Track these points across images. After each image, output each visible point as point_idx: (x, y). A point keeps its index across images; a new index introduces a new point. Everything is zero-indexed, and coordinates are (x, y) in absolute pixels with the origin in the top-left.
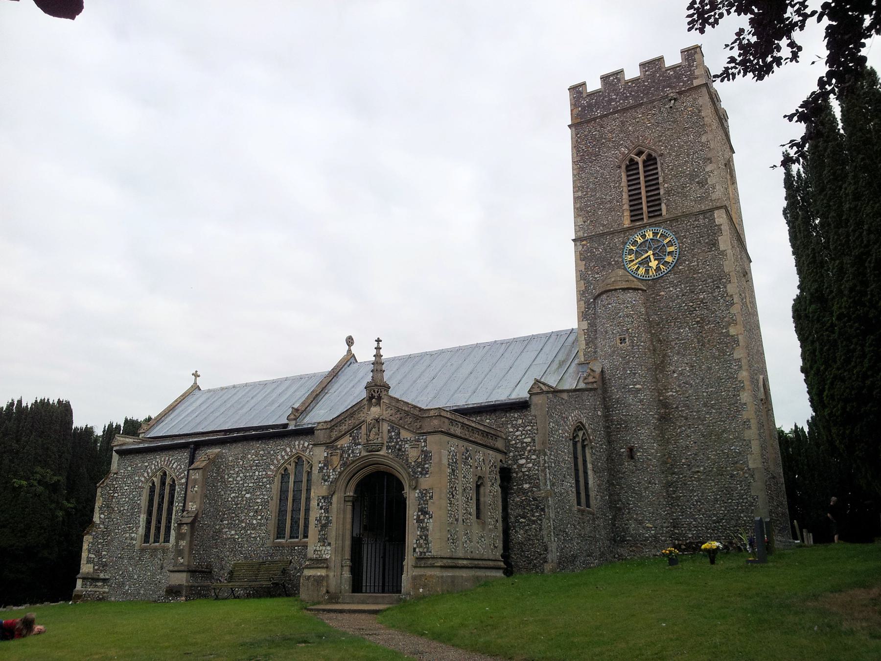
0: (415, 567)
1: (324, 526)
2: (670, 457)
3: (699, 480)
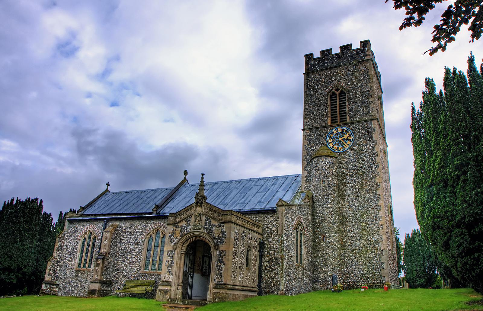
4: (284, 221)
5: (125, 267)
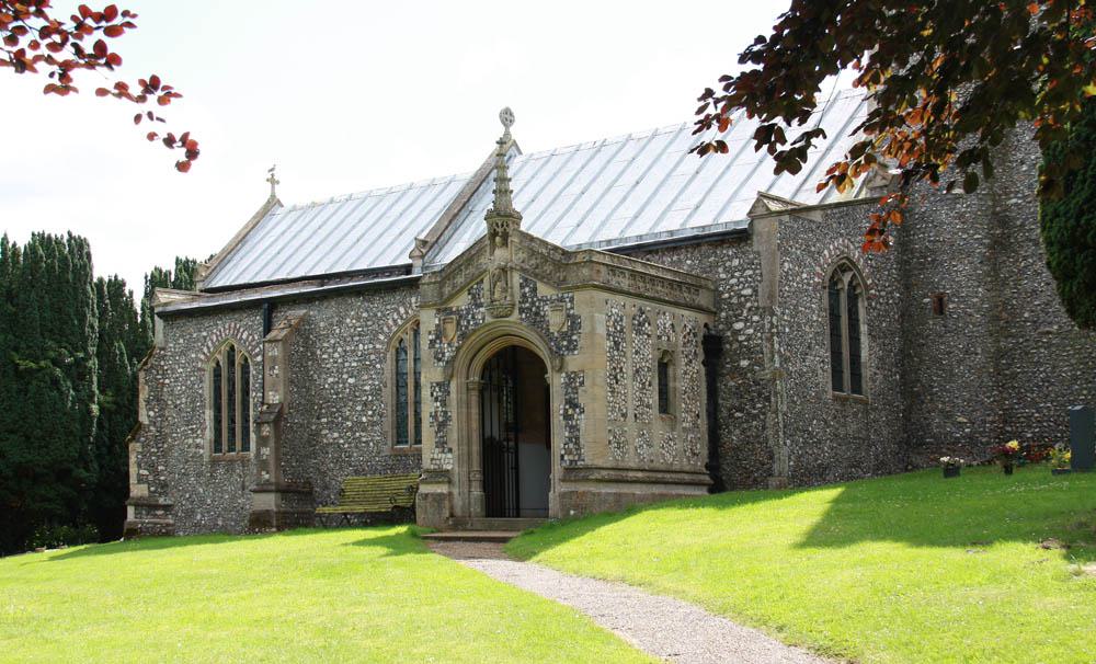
0: (563, 480)
1: (442, 426)
2: (1005, 309)
3: (1049, 346)
4: (778, 261)
5: (342, 441)
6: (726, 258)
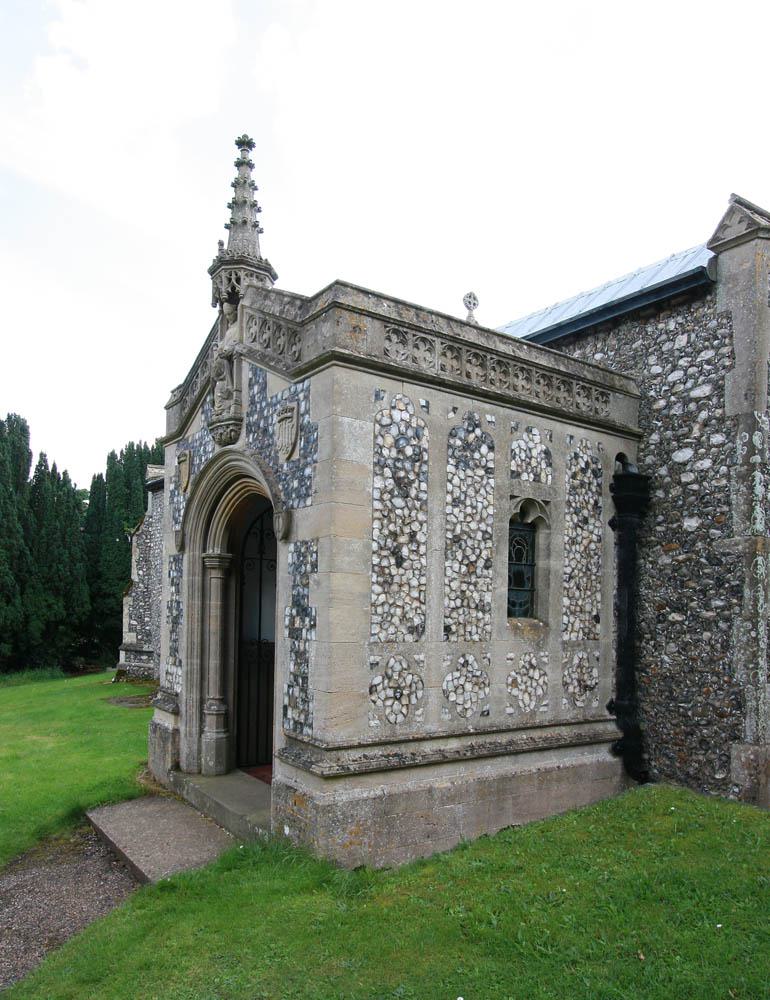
6: (664, 337)
